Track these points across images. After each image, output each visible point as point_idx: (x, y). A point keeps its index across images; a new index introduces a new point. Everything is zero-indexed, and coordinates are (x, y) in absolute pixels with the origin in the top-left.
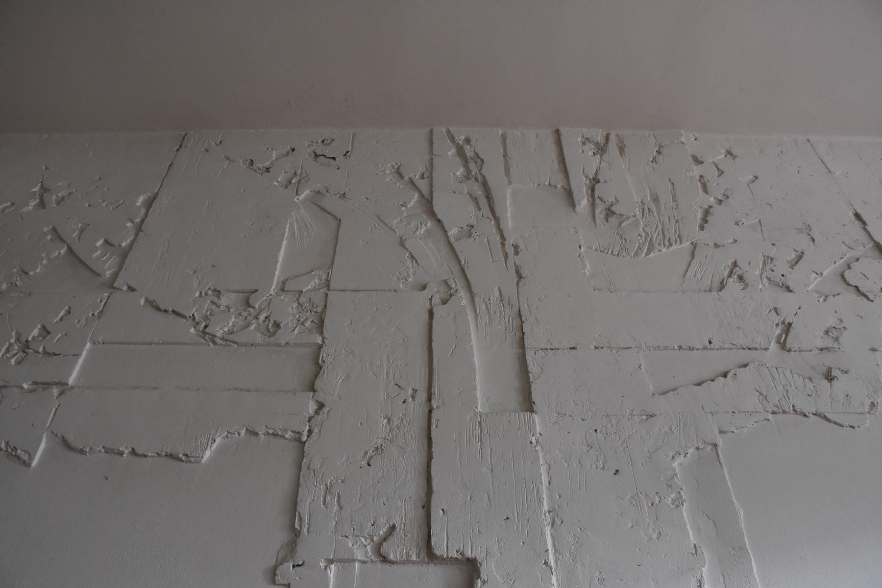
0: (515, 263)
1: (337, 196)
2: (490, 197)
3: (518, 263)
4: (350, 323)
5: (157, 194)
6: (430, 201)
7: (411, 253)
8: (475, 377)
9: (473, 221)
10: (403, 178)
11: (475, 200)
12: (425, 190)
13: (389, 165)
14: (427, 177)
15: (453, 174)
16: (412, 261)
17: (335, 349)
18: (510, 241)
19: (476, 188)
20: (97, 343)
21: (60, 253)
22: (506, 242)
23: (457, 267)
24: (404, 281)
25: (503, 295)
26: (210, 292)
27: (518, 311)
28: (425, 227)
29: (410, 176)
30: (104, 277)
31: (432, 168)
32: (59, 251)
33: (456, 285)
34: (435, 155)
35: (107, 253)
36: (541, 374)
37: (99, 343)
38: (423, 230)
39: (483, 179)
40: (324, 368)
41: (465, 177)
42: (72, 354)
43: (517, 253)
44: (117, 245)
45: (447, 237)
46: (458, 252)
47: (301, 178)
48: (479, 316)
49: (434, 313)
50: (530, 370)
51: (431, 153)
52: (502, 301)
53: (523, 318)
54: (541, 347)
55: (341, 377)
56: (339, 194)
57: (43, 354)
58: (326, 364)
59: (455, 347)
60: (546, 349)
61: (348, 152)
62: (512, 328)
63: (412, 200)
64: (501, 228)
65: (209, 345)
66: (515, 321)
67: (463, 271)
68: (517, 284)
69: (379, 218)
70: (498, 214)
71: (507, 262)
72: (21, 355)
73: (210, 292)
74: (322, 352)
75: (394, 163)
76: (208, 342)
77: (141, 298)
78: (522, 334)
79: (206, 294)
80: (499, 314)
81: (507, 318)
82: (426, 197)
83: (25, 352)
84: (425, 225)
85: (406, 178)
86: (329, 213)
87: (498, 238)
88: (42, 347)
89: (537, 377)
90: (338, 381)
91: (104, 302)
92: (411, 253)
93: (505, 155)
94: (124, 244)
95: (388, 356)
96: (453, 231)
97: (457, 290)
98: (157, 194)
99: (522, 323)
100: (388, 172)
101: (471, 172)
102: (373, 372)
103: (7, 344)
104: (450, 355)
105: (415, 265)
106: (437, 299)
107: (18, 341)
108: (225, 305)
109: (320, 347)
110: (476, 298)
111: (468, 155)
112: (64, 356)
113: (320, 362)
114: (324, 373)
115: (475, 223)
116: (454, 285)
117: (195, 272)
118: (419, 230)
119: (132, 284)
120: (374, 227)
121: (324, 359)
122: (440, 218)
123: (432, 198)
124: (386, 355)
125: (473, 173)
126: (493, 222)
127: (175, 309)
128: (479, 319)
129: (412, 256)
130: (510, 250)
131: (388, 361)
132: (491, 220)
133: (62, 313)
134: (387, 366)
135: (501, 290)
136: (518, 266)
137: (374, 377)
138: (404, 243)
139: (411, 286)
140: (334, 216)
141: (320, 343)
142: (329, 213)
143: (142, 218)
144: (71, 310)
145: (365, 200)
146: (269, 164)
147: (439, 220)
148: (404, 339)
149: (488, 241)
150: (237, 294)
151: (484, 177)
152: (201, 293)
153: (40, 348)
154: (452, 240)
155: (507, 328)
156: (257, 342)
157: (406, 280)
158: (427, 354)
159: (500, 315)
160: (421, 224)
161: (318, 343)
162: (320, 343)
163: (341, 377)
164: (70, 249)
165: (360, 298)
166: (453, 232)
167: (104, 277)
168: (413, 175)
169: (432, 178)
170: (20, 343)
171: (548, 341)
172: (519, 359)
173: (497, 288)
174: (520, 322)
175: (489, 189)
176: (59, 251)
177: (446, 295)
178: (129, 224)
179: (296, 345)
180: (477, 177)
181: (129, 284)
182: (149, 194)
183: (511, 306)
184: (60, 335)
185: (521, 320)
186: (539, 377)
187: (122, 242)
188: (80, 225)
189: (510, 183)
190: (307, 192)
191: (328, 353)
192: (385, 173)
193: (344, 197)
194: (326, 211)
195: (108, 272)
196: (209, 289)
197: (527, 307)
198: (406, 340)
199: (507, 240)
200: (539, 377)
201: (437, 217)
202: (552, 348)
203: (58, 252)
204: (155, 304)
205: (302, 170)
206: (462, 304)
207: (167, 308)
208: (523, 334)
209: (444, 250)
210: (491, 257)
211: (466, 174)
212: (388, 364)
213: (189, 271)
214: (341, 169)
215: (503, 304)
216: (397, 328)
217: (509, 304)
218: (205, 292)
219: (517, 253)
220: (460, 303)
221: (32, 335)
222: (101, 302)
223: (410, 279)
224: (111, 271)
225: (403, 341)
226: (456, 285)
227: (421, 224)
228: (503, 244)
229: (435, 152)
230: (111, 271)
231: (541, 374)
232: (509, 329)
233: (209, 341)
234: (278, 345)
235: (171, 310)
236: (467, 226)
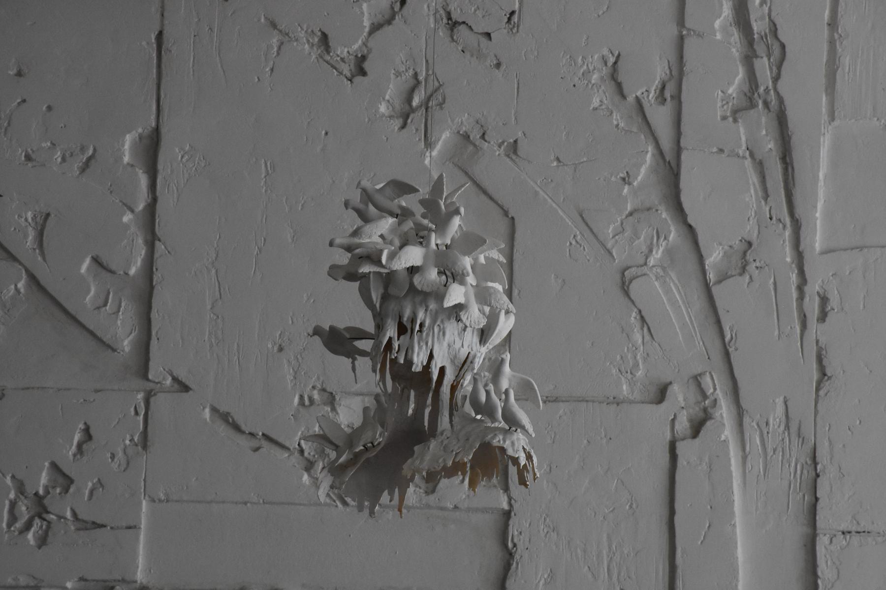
0: (817, 342)
1: (502, 148)
2: (788, 159)
3: (823, 340)
4: (548, 470)
5: (157, 130)
6: (673, 164)
7: (640, 311)
8: (736, 586)
9: (750, 230)
10: (624, 97)
11: (760, 167)
12: (667, 144)
13: (596, 57)
14: (672, 97)
15: (722, 92)
16: (642, 329)
17: (529, 520)
18: (813, 288)
19: (764, 132)
20: (157, 501)
21: (17, 290)
22: (807, 289)
23: (718, 343)
24: (629, 376)
25: (790, 415)
26: (316, 396)
27: (813, 450)
28: (666, 241)
29: (639, 94)
30: (122, 353)
31: (681, 73)
32: (16, 286)
33: (715, 389)
34: (689, 30)
35: (109, 293)
36: (835, 581)
37: (160, 501)
38: (661, 249)
39: (781, 107)
40: (517, 557)
41: (745, 94)
42: (124, 524)
43: (823, 316)
44: (122, 273)
45: (704, 272)
46: (721, 312)
47: (429, 92)
48: (749, 458)
49: (677, 455)
50: (819, 573)
51: (681, 22)
52: (787, 427)
53: (819, 467)
54: (844, 527)
55: (543, 575)
56: (506, 144)
57: (74, 521)
58: (519, 551)
59: (709, 527)
60: (849, 532)
61: (513, 13)
62: (800, 484)
63: (641, 165)
64: (801, 249)
65: (337, 506)
66: (805, 472)
67: (727, 355)
68: (818, 389)
69: (581, 216)
70: (799, 211)
71: (805, 338)
72: (39, 524)
73: (316, 396)
74: (510, 528)
75: (605, 52)
76: (335, 501)
77: (204, 408)
78: (814, 499)
79: (311, 399)
80: (781, 454)
81: (793, 464)
82: (668, 160)
83: (44, 520)
84: (665, 238)
85: (631, 99)
86: (491, 198)
87: (794, 277)
88: (69, 509)
89: (830, 585)
90: (539, 582)
91: (143, 413)
92: (640, 311)
93: (833, 24)
94: (132, 271)
95: (609, 537)
96: (715, 255)
97: (715, 400)
98: (157, 130)
99: (818, 476)
100: (595, 77)
101: (757, 87)
102: (589, 567)
103: (7, 502)
104: (702, 542)
105: (647, 337)
106: (683, 425)
107: (22, 494)
108: (346, 423)
109: (507, 515)
110: (746, 420)
111: (755, 28)
112: (112, 528)
113: (510, 545)
114: (517, 568)
115: (754, 237)
116: (712, 390)
117: (281, 349)
118: (654, 252)
119: (183, 376)
120: (574, 242)
121: (515, 540)
122: (693, 224)
123: (679, 165)
124: (605, 535)
125: (762, 89)
126: (788, 233)
127: (265, 432)
128: (749, 465)
129: (642, 318)
130: (813, 307)
131: (610, 548)
132: (784, 227)
133: (77, 437)
134: (608, 556)
135: (789, 403)
136: (821, 348)
137: (590, 576)
138: (628, 287)
139: (642, 387)
140: (501, 207)
141: (506, 506)
142: (491, 198)
143: (146, 201)
144: (92, 432)
145: (555, 164)
146: (360, 47)
147: (690, 226)
148: (632, 504)
149: (775, 284)
150: (361, 397)
151: (781, 100)
152: (301, 397)
153: (66, 512)
154: (712, 276)
155: (792, 486)
156: (411, 504)
157: (631, 373)
158: (666, 536)
159: (783, 456)
160: (658, 238)
161: (503, 509)
162: (506, 506)
163: (543, 575)
164: (32, 278)
165: (560, 417)
166: (714, 258)
167: (122, 353)
168: (644, 90)
169: (680, 103)
170: (26, 497)
171: (854, 517)
172: (805, 546)
173: (782, 398)
174: (814, 474)
175: (790, 138)
176: (16, 286)
177: (697, 409)
178: (127, 218)
179: (469, 510)
180: (769, 100)
181: (175, 375)
182: (140, 130)
183: (801, 440)
184: (90, 484)
185: (816, 469)
186: (832, 586)
187: (129, 268)
188: (30, 215)
189: (832, 117)
190: (446, 135)
191: (520, 530)
192: (590, 82)
193: (515, 152)
194: (485, 192)
195: (126, 343)
196: (314, 387)
197: (827, 444)
198: (634, 506)
199: (809, 284)
200: (832, 586)
201: (686, 219)
202: (859, 530)
203: (13, 287)
204: (231, 420)
205: (427, 70)
206: (722, 439)
207: (253, 431)
208: (817, 499)
209: (698, 302)
210: (776, 327)
211: (746, 88)
212: (610, 551)
213: (270, 346)
214: (503, 67)
215: (789, 434)
216: (622, 482)
217: (799, 437)
218: (308, 396)
219: (823, 316)
220: (719, 437)
221: (41, 485)
222: (137, 413)
223: (640, 373)
224: (131, 337)
225: (631, 507)
226: (715, 389)
227: (658, 238)
228: (800, 289)
229: (689, 24)
230: (131, 337)
231: (835, 581)
232: (795, 486)
233: (335, 498)
234: (442, 509)
235: (260, 434)
236: (741, 241)
